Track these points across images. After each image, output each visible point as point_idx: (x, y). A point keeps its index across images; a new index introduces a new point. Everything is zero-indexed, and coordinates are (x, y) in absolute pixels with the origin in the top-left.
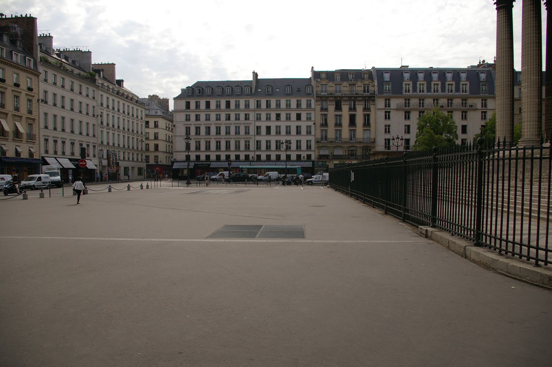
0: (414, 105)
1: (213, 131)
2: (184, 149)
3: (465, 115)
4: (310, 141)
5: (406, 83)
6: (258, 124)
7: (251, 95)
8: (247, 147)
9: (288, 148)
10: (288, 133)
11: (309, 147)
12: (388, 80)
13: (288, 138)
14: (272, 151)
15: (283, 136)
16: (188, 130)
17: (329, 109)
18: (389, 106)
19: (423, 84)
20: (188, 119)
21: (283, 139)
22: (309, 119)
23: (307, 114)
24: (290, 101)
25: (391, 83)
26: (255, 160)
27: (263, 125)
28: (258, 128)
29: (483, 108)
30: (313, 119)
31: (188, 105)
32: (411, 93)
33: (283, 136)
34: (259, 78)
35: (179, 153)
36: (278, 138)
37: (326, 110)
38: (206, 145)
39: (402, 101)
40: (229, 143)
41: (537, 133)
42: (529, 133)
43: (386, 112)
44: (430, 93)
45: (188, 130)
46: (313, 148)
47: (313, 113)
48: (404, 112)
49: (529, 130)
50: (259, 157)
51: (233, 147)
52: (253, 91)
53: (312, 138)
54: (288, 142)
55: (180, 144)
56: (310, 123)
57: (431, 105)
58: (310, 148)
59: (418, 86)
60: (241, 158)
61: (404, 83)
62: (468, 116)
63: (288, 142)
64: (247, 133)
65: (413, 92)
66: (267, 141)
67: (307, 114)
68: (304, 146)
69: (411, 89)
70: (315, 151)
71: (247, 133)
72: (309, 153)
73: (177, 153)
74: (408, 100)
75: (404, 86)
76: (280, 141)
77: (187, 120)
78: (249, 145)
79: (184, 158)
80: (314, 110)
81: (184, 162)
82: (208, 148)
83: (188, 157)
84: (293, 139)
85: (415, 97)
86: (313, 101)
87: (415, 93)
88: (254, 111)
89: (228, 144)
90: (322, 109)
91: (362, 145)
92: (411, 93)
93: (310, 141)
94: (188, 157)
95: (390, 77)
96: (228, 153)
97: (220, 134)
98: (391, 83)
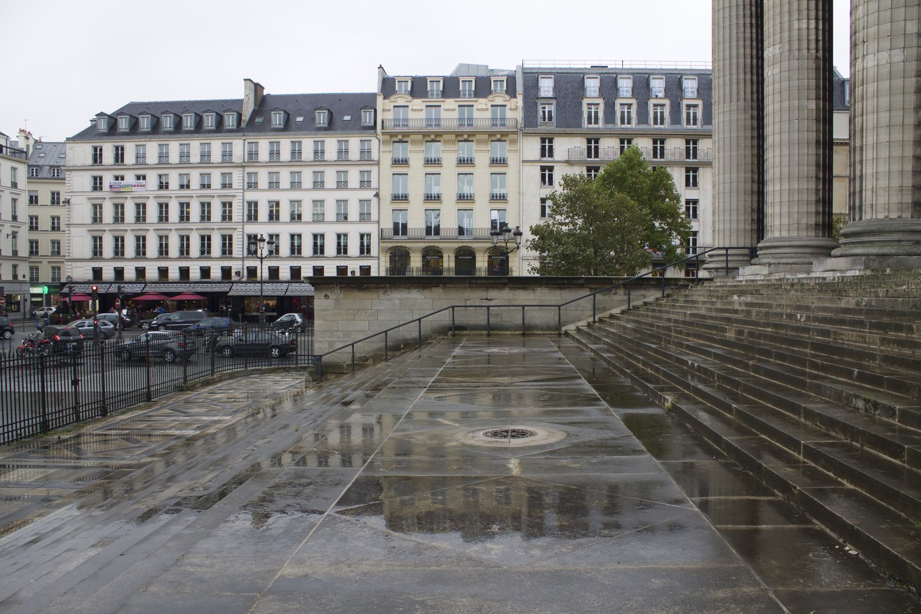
0: (673, 154)
1: (195, 212)
2: (89, 254)
3: (695, 178)
4: (369, 235)
5: (590, 101)
6: (251, 196)
7: (239, 129)
8: (227, 249)
9: (274, 252)
10: (274, 216)
11: (365, 250)
12: (550, 94)
13: (274, 228)
14: (328, 258)
15: (352, 222)
16: (97, 209)
17: (411, 162)
18: (551, 155)
19: (630, 105)
20: (97, 183)
21: (262, 229)
22: (365, 184)
23: (160, 176)
24: (300, 143)
25: (554, 102)
26: (245, 279)
27: (263, 199)
28: (318, 203)
29: (547, 158)
30: (374, 184)
31: (97, 156)
32: (601, 124)
33: (352, 222)
34: (265, 93)
35: (78, 264)
36: (251, 229)
37: (405, 162)
38: (138, 246)
39: (580, 144)
40: (123, 240)
41: (812, 221)
42: (785, 221)
43: (543, 169)
44: (645, 126)
45: (97, 209)
46: (374, 251)
47: (374, 170)
48: (683, 170)
49: (785, 209)
50: (252, 272)
51: (174, 250)
52: (243, 125)
53: (372, 229)
54: (274, 239)
55: (78, 244)
56: (369, 194)
57: (681, 154)
58: (369, 251)
59: (618, 109)
60: (212, 275)
61: (585, 102)
62: (700, 180)
63: (274, 239)
64: (227, 217)
65: (672, 123)
66: (315, 236)
67: (160, 176)
68: (354, 248)
69: (634, 115)
70: (378, 258)
71: (227, 217)
72: (365, 263)
73: (74, 264)
74: (593, 142)
75: (585, 109)
76: (256, 236)
77: (95, 189)
78: (167, 245)
79: (89, 276)
80: (378, 163)
81: (89, 282)
82: (141, 251)
83: (97, 272)
84: (284, 230)
85: (611, 135)
86: (375, 143)
87: (611, 126)
88: (242, 166)
89: (141, 243)
90: (396, 162)
91: (390, 245)
92: (601, 124)
93: (369, 235)
94: (97, 272)
95: (555, 88)
96: (184, 264)
97: (209, 218)
98: (554, 102)
